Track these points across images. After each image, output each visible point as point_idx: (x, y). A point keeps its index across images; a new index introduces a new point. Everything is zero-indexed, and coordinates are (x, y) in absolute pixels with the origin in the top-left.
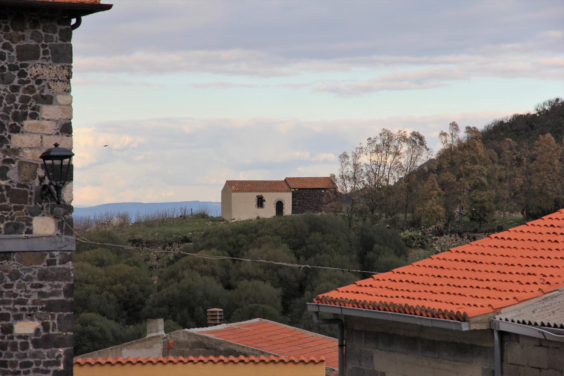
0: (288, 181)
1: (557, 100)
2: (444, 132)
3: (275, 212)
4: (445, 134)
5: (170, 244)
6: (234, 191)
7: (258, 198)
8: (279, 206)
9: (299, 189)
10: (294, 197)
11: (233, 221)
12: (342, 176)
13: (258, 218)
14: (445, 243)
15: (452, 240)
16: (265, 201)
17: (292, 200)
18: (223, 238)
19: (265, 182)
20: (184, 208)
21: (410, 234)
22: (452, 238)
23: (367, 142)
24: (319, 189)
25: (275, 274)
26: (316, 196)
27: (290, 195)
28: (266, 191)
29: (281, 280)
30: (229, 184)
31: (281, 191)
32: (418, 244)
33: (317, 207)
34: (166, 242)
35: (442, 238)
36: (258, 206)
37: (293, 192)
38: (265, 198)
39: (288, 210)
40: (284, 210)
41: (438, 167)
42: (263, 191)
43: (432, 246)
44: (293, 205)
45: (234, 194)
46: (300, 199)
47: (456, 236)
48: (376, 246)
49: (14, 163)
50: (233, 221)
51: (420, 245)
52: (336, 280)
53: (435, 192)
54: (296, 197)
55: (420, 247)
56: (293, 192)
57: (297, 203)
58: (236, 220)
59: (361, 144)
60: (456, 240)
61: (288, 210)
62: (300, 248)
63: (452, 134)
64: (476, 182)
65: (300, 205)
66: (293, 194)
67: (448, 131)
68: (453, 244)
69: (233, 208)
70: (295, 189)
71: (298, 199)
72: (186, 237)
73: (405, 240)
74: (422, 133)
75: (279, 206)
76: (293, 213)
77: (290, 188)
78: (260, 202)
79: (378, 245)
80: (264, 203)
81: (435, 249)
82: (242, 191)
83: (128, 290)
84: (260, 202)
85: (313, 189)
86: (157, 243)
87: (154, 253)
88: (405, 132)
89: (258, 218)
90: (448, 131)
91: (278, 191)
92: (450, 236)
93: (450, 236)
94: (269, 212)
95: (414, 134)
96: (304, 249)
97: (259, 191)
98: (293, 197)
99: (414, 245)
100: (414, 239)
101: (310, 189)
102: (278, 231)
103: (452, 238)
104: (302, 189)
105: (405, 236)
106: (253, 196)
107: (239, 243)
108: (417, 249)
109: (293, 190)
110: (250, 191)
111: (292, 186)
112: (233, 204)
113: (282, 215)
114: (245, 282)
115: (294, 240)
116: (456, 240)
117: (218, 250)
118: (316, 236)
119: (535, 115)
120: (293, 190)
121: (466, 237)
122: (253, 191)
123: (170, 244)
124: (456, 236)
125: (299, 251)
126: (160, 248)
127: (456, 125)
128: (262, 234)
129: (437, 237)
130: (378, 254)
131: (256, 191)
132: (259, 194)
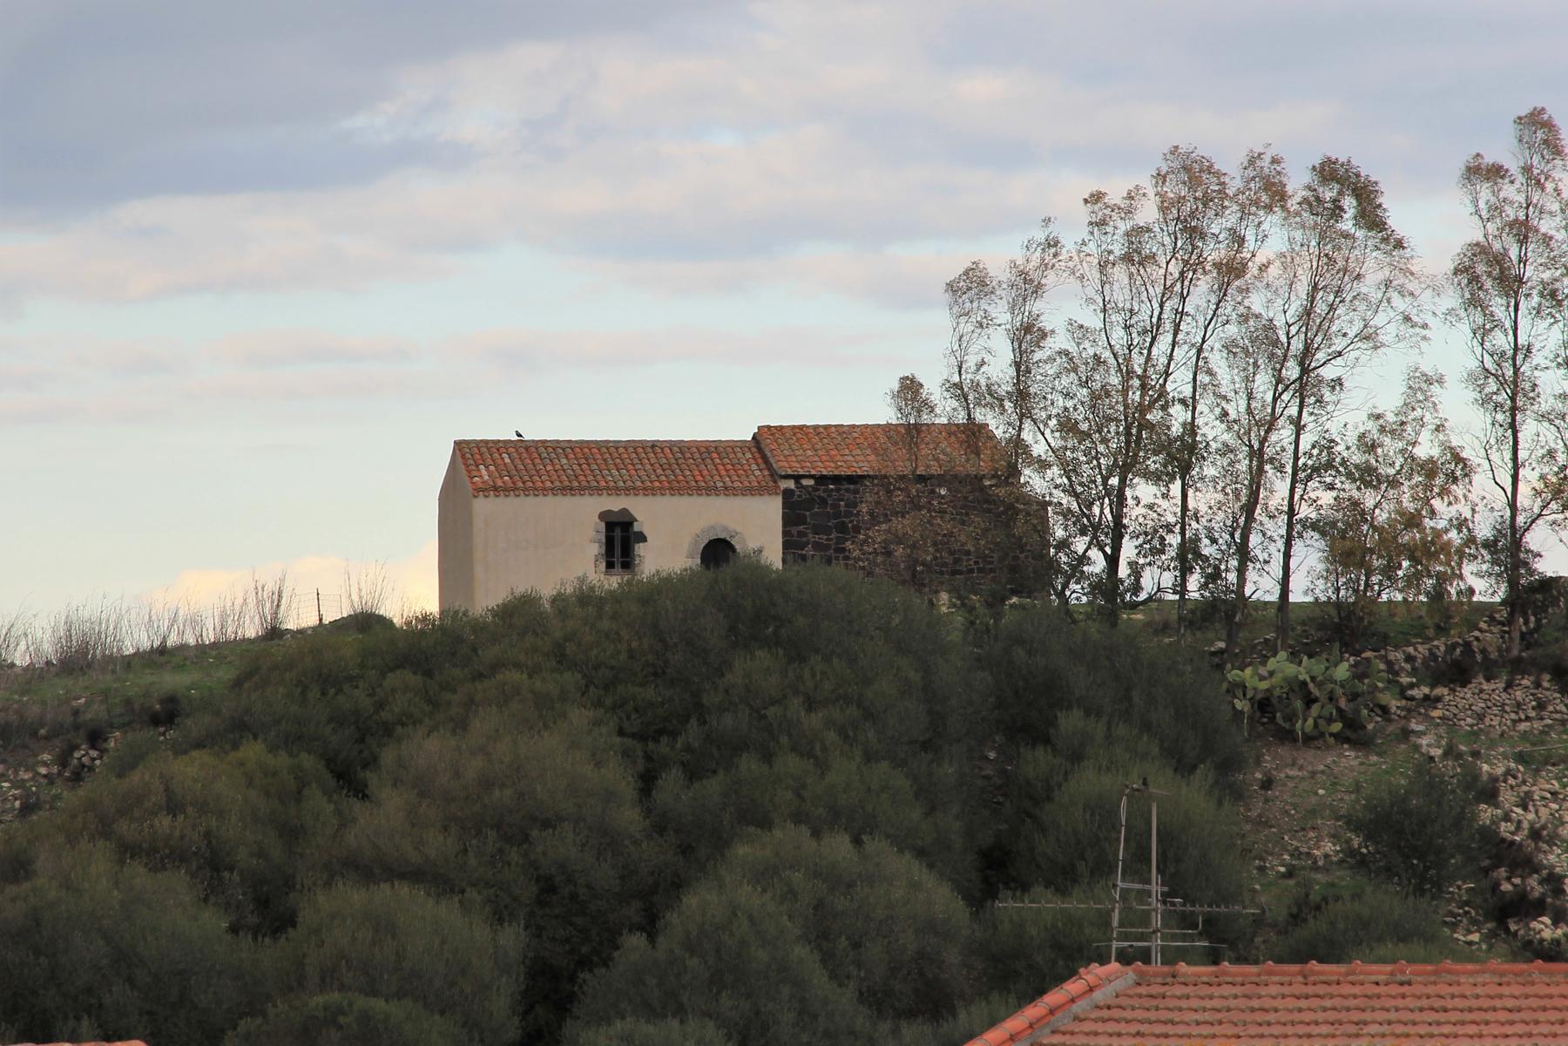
0: (769, 445)
2: (1489, 159)
4: (1496, 173)
5: (96, 738)
6: (481, 490)
9: (821, 480)
12: (959, 386)
14: (1481, 717)
15: (1519, 705)
16: (642, 538)
17: (785, 533)
18: (314, 693)
19: (654, 445)
20: (271, 586)
21: (1291, 669)
22: (1519, 695)
23: (1083, 214)
28: (648, 491)
29: (548, 887)
30: (468, 454)
31: (728, 491)
32: (1330, 720)
34: (77, 727)
35: (1466, 695)
36: (610, 565)
37: (787, 494)
38: (643, 524)
42: (629, 490)
43: (1406, 734)
46: (826, 530)
47: (1538, 685)
48: (1070, 722)
49: (454, 691)
51: (1337, 727)
52: (797, 877)
54: (801, 520)
55: (1340, 738)
56: (787, 494)
59: (1047, 221)
60: (1541, 706)
62: (674, 735)
63: (1527, 170)
66: (787, 504)
67: (1504, 150)
68: (1523, 726)
69: (479, 572)
70: (797, 478)
71: (817, 530)
73: (1264, 705)
74: (1367, 168)
77: (775, 476)
79: (1077, 714)
80: (640, 549)
81: (1417, 748)
82: (527, 491)
84: (620, 540)
86: (34, 734)
87: (15, 785)
88: (1275, 161)
90: (1504, 150)
91: (711, 490)
92: (1509, 686)
93: (1509, 686)
95: (1329, 172)
96: (693, 733)
97: (615, 491)
98: (788, 521)
99: (1305, 725)
100: (1310, 701)
102: (570, 649)
103: (1519, 695)
104: (836, 479)
105: (1264, 685)
106: (582, 518)
108: (1328, 748)
109: (791, 484)
110: (567, 490)
111: (782, 466)
114: (352, 896)
115: (650, 693)
116: (1541, 706)
117: (273, 749)
118: (757, 668)
120: (791, 484)
122: (582, 490)
123: (96, 738)
124: (1538, 685)
125: (663, 747)
126: (46, 757)
127: (1549, 125)
128: (496, 667)
129: (1441, 691)
130: (1077, 757)
131: (598, 491)
132: (615, 504)
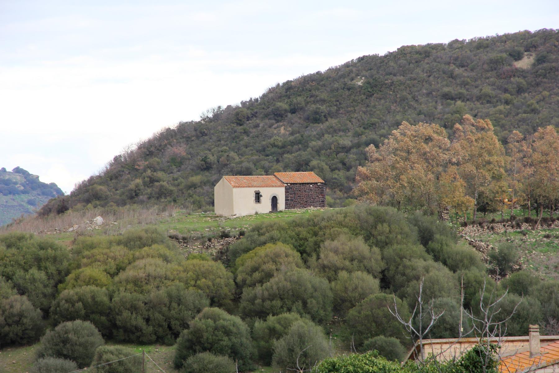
1: (219, 107)
3: (271, 207)
6: (235, 187)
7: (256, 194)
8: (274, 200)
9: (291, 184)
10: (287, 192)
11: (235, 217)
13: (257, 213)
16: (261, 196)
24: (308, 184)
25: (362, 265)
26: (305, 191)
27: (283, 189)
28: (262, 187)
33: (306, 202)
39: (281, 205)
40: (278, 205)
41: (8, 180)
43: (462, 236)
44: (286, 200)
45: (235, 190)
50: (235, 217)
53: (458, 184)
57: (289, 198)
58: (237, 216)
61: (281, 205)
64: (494, 173)
65: (292, 200)
66: (286, 189)
69: (234, 203)
70: (287, 184)
72: (224, 232)
75: (274, 200)
76: (286, 208)
78: (258, 197)
80: (261, 198)
83: (214, 285)
84: (258, 197)
85: (303, 184)
86: (193, 239)
89: (257, 213)
92: (473, 227)
93: (473, 227)
94: (265, 207)
101: (300, 184)
104: (294, 184)
107: (301, 236)
112: (234, 199)
113: (277, 210)
119: (199, 122)
121: (486, 227)
123: (210, 240)
